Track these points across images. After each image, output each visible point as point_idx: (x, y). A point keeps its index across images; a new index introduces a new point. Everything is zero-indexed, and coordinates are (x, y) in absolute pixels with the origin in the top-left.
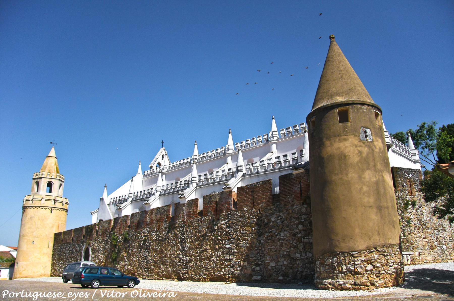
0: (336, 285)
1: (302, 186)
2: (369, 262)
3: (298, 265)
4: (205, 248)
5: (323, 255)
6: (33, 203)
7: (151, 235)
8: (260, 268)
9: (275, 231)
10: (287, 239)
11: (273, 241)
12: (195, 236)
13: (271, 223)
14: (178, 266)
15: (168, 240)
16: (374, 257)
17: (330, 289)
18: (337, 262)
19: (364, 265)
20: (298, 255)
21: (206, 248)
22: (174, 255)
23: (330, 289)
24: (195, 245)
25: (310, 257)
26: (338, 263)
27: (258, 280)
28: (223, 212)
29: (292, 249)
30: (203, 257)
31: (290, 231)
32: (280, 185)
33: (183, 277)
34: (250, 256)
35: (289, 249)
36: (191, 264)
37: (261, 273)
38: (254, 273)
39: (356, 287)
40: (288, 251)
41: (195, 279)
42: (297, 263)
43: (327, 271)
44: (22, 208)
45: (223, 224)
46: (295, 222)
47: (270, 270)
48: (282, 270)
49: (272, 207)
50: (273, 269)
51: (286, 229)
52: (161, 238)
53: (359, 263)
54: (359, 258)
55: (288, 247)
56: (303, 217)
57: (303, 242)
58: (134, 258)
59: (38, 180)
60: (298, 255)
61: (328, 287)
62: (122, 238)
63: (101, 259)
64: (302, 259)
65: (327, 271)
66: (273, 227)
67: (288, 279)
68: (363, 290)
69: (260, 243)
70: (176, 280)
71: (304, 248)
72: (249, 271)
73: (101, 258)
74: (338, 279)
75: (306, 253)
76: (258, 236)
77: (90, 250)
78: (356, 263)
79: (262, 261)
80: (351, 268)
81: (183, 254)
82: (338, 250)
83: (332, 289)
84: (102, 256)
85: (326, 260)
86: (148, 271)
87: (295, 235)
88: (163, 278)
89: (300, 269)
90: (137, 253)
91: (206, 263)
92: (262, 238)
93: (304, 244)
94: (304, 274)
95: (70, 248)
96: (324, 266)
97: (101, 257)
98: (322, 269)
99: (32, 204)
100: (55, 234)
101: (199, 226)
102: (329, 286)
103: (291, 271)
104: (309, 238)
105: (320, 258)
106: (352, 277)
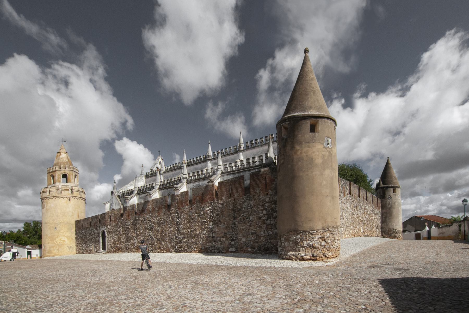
0: (299, 256)
1: (267, 181)
2: (323, 239)
3: (262, 240)
4: (194, 228)
5: (288, 233)
6: (50, 194)
7: (154, 219)
8: (235, 242)
9: (246, 215)
10: (254, 221)
11: (245, 223)
12: (187, 219)
13: (243, 209)
14: (175, 242)
15: (167, 223)
16: (327, 235)
17: (294, 260)
18: (300, 238)
19: (320, 241)
20: (262, 233)
21: (195, 229)
22: (172, 234)
23: (294, 260)
24: (187, 226)
25: (271, 235)
26: (301, 239)
27: (233, 251)
28: (208, 201)
29: (258, 228)
30: (193, 235)
31: (257, 215)
32: (250, 179)
33: (179, 250)
34: (228, 233)
35: (255, 229)
36: (184, 240)
37: (235, 246)
38: (230, 246)
39: (314, 258)
40: (255, 230)
41: (188, 251)
42: (261, 239)
43: (290, 245)
44: (41, 199)
45: (208, 210)
46: (261, 209)
47: (241, 244)
48: (250, 244)
49: (244, 197)
50: (244, 243)
51: (254, 214)
52: (161, 222)
53: (316, 239)
54: (317, 236)
55: (255, 227)
56: (267, 204)
57: (266, 224)
58: (141, 237)
59: (52, 173)
60: (262, 233)
61: (292, 258)
62: (131, 222)
63: (115, 239)
64: (265, 236)
65: (290, 245)
66: (244, 212)
67: (254, 250)
68: (318, 260)
69: (235, 224)
70: (173, 252)
71: (267, 228)
72: (227, 245)
73: (115, 238)
74: (300, 252)
75: (268, 231)
76: (233, 219)
77: (106, 233)
78: (314, 240)
79: (236, 237)
80: (310, 243)
81: (178, 233)
82: (301, 229)
83: (295, 259)
84: (116, 236)
85: (291, 237)
86: (152, 246)
87: (260, 218)
88: (164, 251)
89: (263, 243)
90: (143, 233)
91: (195, 239)
92: (236, 221)
93: (266, 225)
94: (266, 246)
95: (89, 231)
96: (288, 242)
97: (115, 237)
98: (287, 244)
99: (49, 195)
100: (76, 221)
101: (190, 212)
102: (293, 257)
103: (257, 244)
104: (270, 221)
105: (286, 236)
106: (311, 250)
